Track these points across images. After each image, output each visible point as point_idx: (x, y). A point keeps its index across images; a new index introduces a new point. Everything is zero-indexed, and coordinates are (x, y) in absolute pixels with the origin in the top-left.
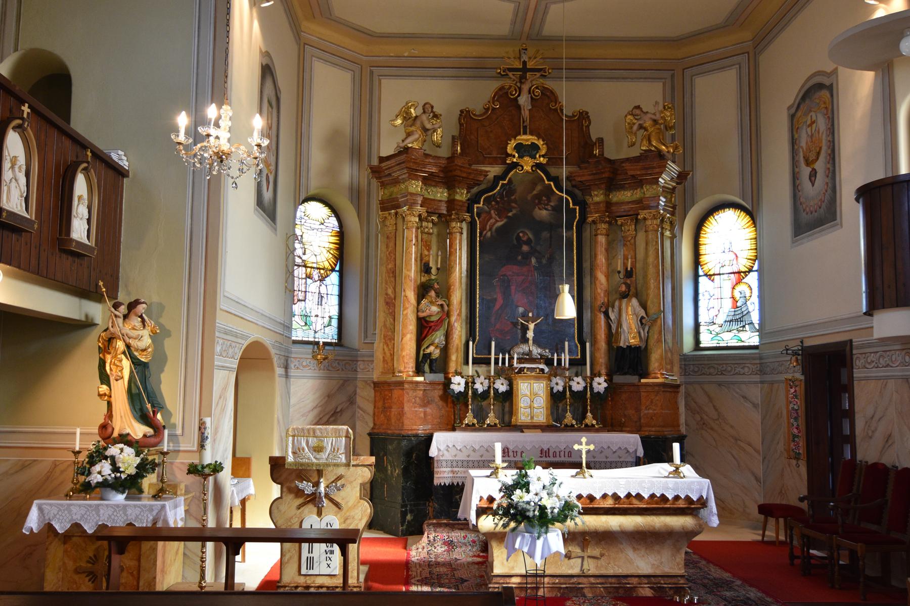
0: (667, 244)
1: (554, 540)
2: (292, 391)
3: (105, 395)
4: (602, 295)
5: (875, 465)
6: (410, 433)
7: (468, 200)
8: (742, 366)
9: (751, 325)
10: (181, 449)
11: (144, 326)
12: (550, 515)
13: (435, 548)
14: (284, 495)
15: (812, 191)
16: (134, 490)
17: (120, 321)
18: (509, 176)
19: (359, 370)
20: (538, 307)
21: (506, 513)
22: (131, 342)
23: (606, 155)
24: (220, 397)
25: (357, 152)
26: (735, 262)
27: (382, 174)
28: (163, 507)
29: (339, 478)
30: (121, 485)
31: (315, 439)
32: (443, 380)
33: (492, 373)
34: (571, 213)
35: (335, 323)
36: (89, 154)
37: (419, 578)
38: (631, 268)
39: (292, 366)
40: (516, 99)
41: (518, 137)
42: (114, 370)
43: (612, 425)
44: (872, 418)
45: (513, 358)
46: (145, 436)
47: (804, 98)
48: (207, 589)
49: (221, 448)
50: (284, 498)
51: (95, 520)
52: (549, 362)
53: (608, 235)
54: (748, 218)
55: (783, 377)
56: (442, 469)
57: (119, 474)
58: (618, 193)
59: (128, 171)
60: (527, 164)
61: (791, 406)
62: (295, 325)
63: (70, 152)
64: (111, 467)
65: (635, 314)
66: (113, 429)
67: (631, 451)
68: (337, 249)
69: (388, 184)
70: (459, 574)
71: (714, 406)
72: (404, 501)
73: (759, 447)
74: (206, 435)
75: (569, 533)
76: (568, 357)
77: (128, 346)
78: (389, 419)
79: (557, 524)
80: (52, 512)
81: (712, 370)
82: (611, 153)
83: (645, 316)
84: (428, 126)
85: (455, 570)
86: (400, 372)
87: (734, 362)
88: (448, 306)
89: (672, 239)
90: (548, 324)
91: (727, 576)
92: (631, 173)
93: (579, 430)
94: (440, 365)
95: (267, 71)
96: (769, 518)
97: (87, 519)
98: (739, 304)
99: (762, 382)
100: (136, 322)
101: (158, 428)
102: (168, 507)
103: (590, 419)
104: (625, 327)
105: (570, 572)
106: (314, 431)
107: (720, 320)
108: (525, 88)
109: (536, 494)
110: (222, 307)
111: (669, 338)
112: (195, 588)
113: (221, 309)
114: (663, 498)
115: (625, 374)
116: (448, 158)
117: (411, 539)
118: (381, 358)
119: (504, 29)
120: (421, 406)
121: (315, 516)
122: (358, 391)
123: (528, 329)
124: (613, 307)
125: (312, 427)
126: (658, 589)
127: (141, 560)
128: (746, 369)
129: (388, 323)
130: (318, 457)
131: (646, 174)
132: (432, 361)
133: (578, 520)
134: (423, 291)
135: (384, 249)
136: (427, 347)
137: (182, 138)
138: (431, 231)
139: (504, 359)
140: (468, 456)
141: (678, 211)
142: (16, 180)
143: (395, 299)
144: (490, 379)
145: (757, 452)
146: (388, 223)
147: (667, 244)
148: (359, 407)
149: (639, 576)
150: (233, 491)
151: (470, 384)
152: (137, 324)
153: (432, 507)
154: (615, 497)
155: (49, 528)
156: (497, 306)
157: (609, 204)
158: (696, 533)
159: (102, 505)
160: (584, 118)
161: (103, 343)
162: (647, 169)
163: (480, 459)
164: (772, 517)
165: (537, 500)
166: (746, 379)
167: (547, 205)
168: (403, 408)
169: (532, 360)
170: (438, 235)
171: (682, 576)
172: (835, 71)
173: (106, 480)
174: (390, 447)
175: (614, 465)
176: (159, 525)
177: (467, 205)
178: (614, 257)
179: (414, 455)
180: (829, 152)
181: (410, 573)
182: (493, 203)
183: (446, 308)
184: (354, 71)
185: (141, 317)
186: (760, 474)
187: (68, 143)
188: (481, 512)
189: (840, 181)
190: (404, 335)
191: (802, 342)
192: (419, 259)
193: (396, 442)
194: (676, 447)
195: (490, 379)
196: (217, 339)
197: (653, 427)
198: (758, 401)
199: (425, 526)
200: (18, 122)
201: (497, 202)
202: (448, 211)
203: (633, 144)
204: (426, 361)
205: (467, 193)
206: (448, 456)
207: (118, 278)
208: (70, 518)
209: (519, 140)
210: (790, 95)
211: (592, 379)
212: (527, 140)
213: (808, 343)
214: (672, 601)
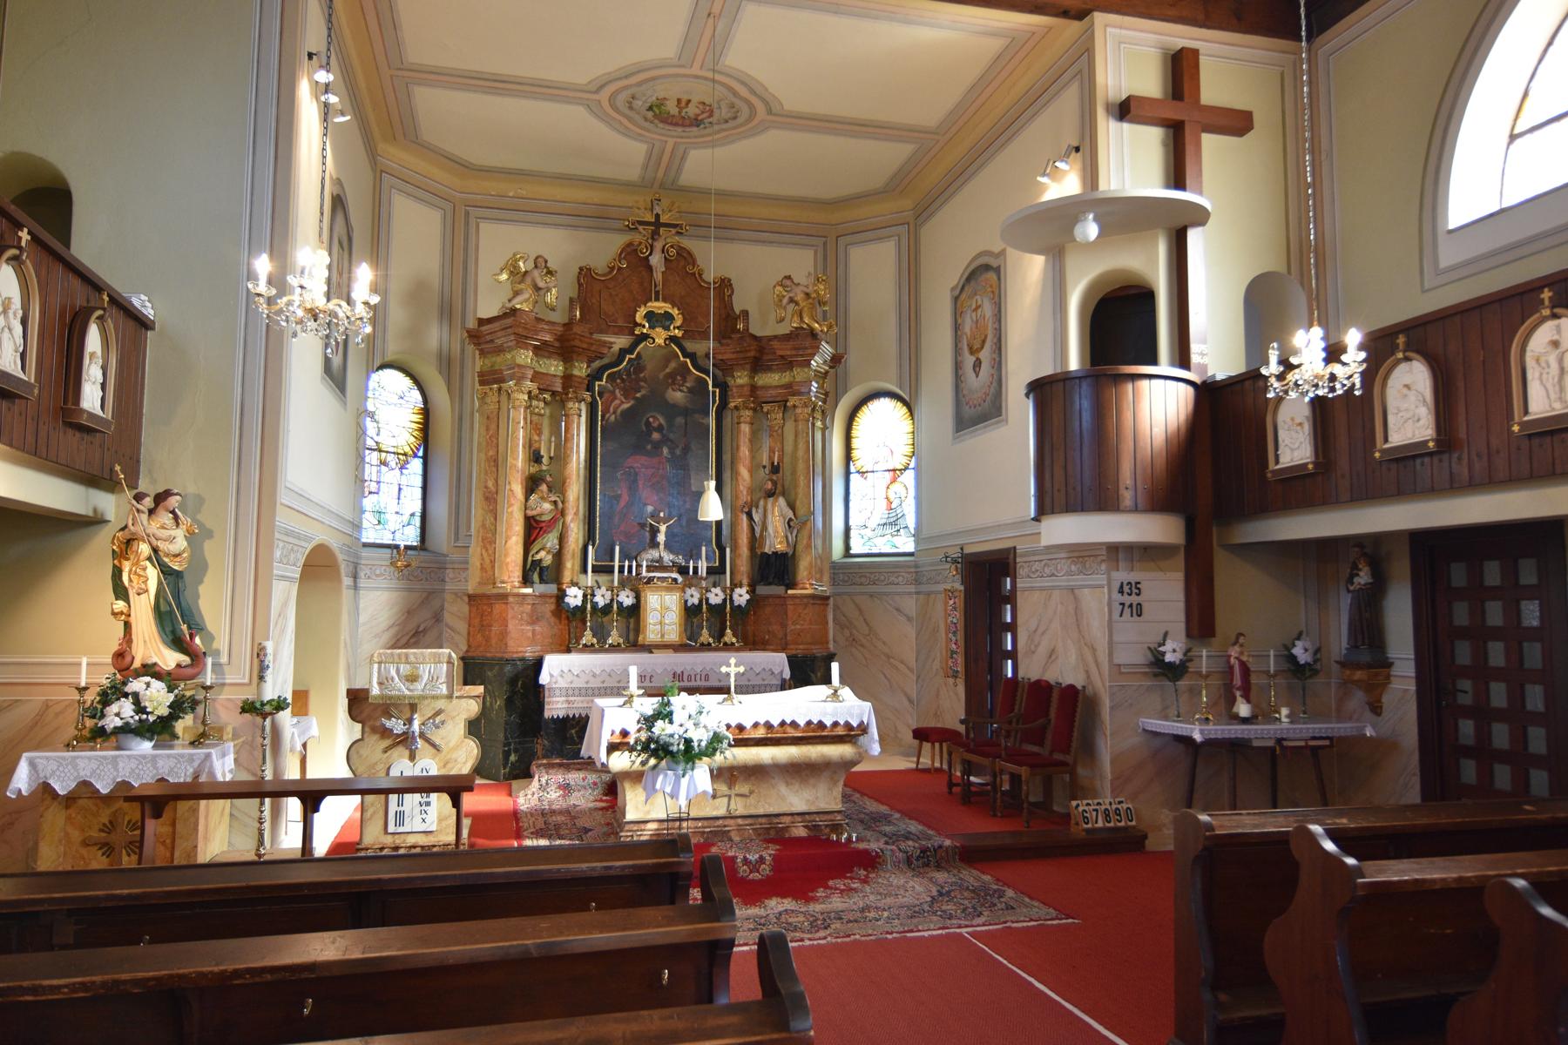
0: (818, 435)
1: (700, 777)
2: (361, 606)
3: (122, 613)
4: (745, 493)
5: (1038, 682)
6: (515, 656)
7: (588, 376)
8: (896, 575)
10: (227, 681)
11: (178, 525)
12: (696, 748)
14: (365, 736)
15: (976, 383)
16: (167, 737)
17: (144, 517)
19: (447, 579)
20: (670, 506)
21: (645, 748)
22: (161, 545)
23: (752, 331)
24: (280, 615)
25: (448, 311)
27: (482, 340)
28: (208, 756)
30: (149, 730)
31: (408, 666)
32: (555, 591)
33: (616, 584)
35: (417, 521)
36: (106, 298)
39: (362, 574)
40: (647, 258)
41: (649, 304)
42: (135, 581)
44: (1035, 631)
45: (642, 566)
46: (179, 666)
47: (968, 280)
48: (266, 858)
49: (280, 680)
50: (366, 740)
51: (111, 776)
52: (683, 571)
54: (905, 410)
55: (941, 587)
56: (554, 699)
57: (145, 716)
58: (764, 375)
59: (153, 322)
60: (660, 336)
61: (950, 619)
62: (365, 524)
63: (80, 295)
64: (133, 707)
65: (782, 515)
66: (133, 658)
68: (420, 430)
69: (488, 353)
70: (580, 823)
72: (506, 738)
73: (913, 664)
74: (266, 663)
75: (720, 770)
76: (705, 565)
77: (155, 550)
78: (488, 639)
79: (705, 759)
80: (49, 768)
81: (863, 580)
82: (756, 330)
84: (541, 284)
85: (575, 818)
86: (504, 582)
89: (824, 430)
90: (681, 526)
91: (883, 809)
92: (780, 353)
93: (717, 649)
95: (338, 203)
96: (924, 743)
97: (99, 775)
98: (893, 506)
99: (917, 593)
100: (167, 518)
101: (197, 656)
102: (214, 757)
103: (729, 637)
104: (770, 529)
105: (715, 813)
106: (407, 656)
107: (873, 524)
108: (658, 245)
109: (681, 725)
110: (283, 501)
111: (819, 542)
112: (251, 857)
113: (282, 504)
114: (821, 725)
115: (770, 584)
116: (565, 325)
117: (515, 784)
118: (478, 564)
119: (633, 174)
121: (406, 761)
122: (446, 605)
123: (658, 531)
124: (757, 507)
125: (389, 651)
127: (177, 826)
128: (901, 579)
130: (411, 687)
131: (797, 356)
132: (542, 569)
133: (728, 753)
134: (532, 484)
135: (484, 433)
136: (537, 553)
137: (262, 287)
138: (542, 411)
139: (630, 567)
140: (587, 683)
141: (830, 397)
142: (10, 329)
143: (497, 493)
144: (612, 591)
145: (911, 670)
146: (488, 400)
147: (818, 435)
148: (447, 625)
149: (792, 814)
150: (293, 734)
152: (167, 522)
153: (541, 744)
154: (768, 726)
155: (46, 789)
156: (622, 504)
157: (754, 388)
158: (854, 763)
159: (122, 756)
161: (119, 546)
162: (799, 349)
163: (602, 685)
165: (681, 733)
166: (899, 589)
169: (663, 568)
170: (552, 416)
171: (839, 812)
172: (1003, 252)
173: (127, 724)
174: (489, 673)
175: (757, 689)
176: (203, 779)
179: (520, 683)
180: (995, 340)
182: (618, 381)
183: (560, 505)
185: (173, 512)
186: (914, 696)
187: (76, 283)
188: (612, 748)
189: (1007, 373)
190: (508, 538)
191: (962, 549)
192: (527, 446)
193: (496, 668)
194: (835, 667)
195: (612, 591)
196: (276, 542)
198: (913, 614)
199: (533, 768)
200: (13, 252)
201: (623, 381)
202: (563, 388)
203: (782, 320)
205: (588, 367)
206: (562, 683)
207: (138, 461)
208: (76, 774)
210: (954, 276)
211: (732, 590)
212: (660, 308)
213: (968, 550)
214: (828, 840)
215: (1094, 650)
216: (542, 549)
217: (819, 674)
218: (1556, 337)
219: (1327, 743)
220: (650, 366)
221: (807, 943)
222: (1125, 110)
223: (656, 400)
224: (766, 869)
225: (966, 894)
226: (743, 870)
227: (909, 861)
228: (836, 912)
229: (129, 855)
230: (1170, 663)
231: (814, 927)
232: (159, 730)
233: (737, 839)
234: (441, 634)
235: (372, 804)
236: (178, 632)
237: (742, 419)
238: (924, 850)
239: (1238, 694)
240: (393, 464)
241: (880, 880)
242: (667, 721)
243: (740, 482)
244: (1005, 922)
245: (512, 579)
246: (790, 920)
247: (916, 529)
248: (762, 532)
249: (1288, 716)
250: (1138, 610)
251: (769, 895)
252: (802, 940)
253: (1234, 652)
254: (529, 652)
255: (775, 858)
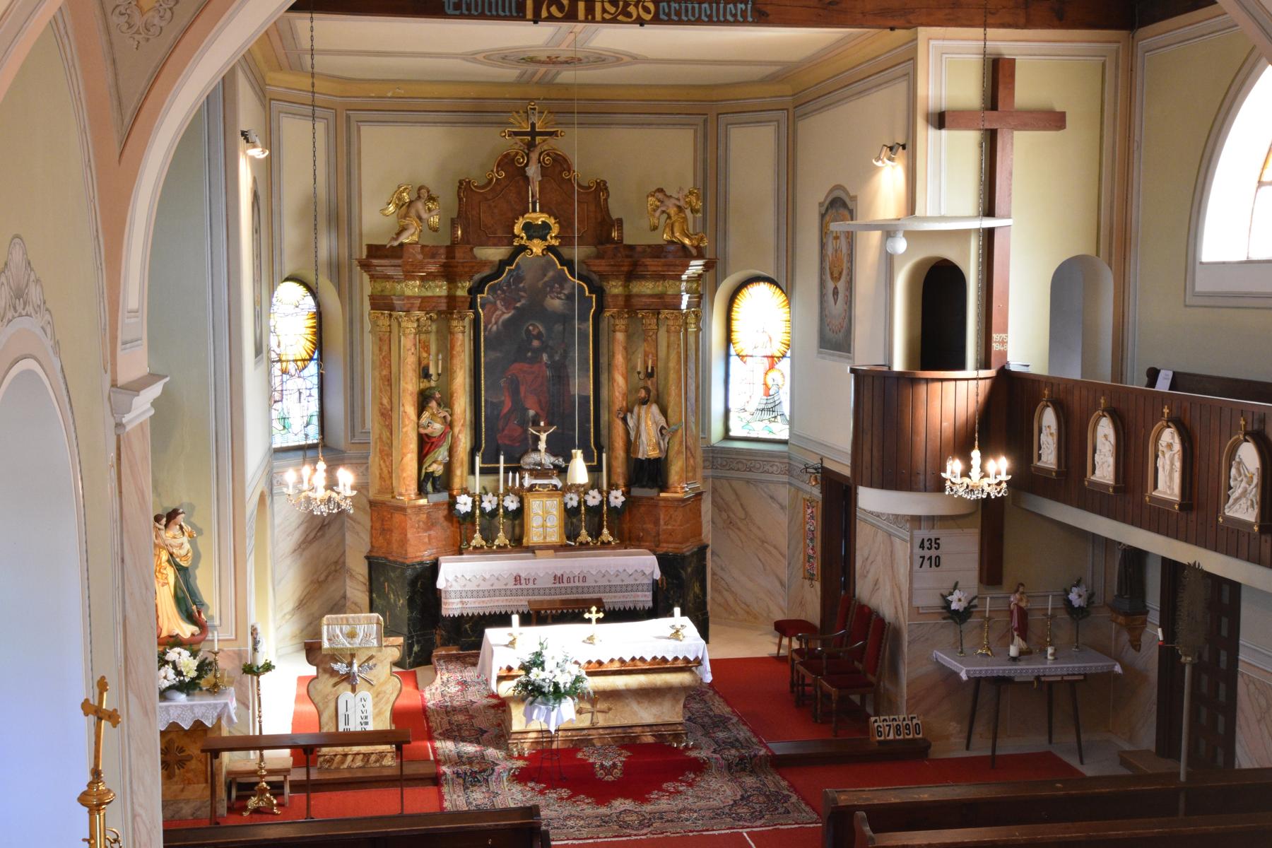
2: (276, 509)
8: (772, 463)
9: (783, 417)
13: (449, 688)
18: (517, 260)
26: (768, 345)
29: (371, 658)
34: (585, 302)
35: (315, 421)
37: (440, 731)
38: (652, 368)
41: (526, 216)
43: (630, 539)
46: (193, 635)
53: (626, 331)
56: (450, 600)
57: (182, 678)
60: (537, 247)
65: (656, 423)
67: (647, 573)
68: (315, 334)
71: (741, 505)
73: (786, 551)
77: (171, 555)
78: (389, 543)
81: (740, 466)
82: (636, 233)
83: (665, 426)
86: (401, 494)
87: (764, 459)
88: (451, 415)
93: (595, 548)
94: (443, 483)
98: (771, 392)
104: (644, 437)
107: (752, 407)
108: (534, 156)
109: (551, 672)
114: (664, 660)
115: (643, 487)
117: (421, 672)
120: (425, 531)
121: (350, 693)
124: (632, 412)
126: (659, 736)
128: (775, 468)
129: (384, 437)
131: (668, 271)
134: (423, 400)
136: (429, 466)
140: (478, 586)
145: (784, 556)
146: (380, 323)
149: (643, 726)
151: (477, 503)
153: (438, 636)
154: (622, 661)
157: (628, 298)
160: (601, 190)
163: (491, 588)
164: (786, 636)
167: (560, 293)
168: (406, 535)
171: (680, 724)
174: (392, 575)
177: (469, 300)
178: (633, 353)
179: (419, 583)
181: (430, 724)
182: (499, 292)
183: (449, 418)
184: (327, 119)
186: (785, 579)
188: (501, 679)
197: (672, 543)
198: (786, 502)
201: (504, 292)
204: (428, 480)
206: (456, 587)
209: (528, 218)
211: (608, 493)
215: (901, 593)
216: (434, 462)
217: (689, 570)
218: (1171, 441)
219: (1082, 678)
220: (529, 277)
221: (634, 838)
222: (940, 120)
223: (535, 310)
224: (617, 773)
225: (761, 799)
226: (600, 773)
227: (729, 767)
228: (661, 813)
229: (179, 769)
230: (954, 610)
231: (642, 825)
232: (188, 687)
233: (598, 744)
234: (343, 524)
235: (327, 724)
236: (190, 611)
237: (617, 328)
238: (742, 758)
239: (1015, 633)
240: (292, 371)
241: (702, 784)
242: (540, 668)
243: (616, 388)
244: (775, 825)
245: (409, 492)
246: (627, 819)
247: (791, 415)
248: (636, 439)
249: (1052, 655)
250: (937, 562)
251: (615, 797)
252: (630, 836)
253: (1014, 599)
254: (426, 555)
255: (624, 763)
